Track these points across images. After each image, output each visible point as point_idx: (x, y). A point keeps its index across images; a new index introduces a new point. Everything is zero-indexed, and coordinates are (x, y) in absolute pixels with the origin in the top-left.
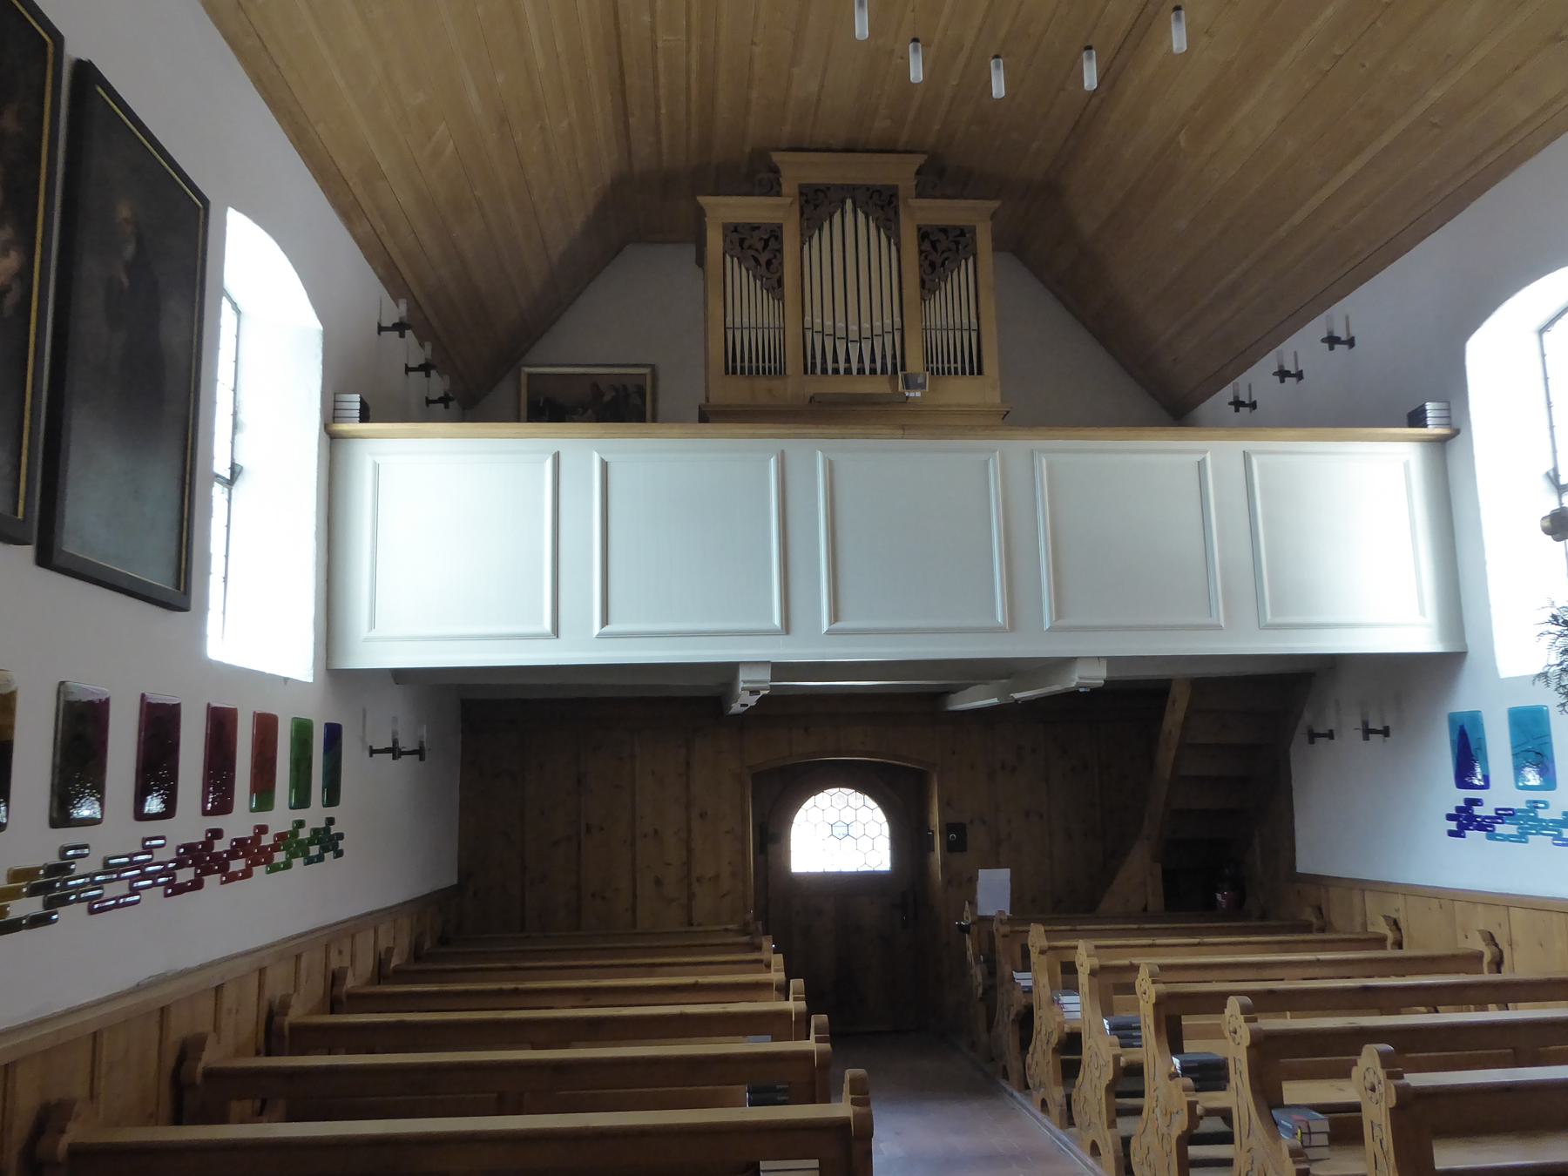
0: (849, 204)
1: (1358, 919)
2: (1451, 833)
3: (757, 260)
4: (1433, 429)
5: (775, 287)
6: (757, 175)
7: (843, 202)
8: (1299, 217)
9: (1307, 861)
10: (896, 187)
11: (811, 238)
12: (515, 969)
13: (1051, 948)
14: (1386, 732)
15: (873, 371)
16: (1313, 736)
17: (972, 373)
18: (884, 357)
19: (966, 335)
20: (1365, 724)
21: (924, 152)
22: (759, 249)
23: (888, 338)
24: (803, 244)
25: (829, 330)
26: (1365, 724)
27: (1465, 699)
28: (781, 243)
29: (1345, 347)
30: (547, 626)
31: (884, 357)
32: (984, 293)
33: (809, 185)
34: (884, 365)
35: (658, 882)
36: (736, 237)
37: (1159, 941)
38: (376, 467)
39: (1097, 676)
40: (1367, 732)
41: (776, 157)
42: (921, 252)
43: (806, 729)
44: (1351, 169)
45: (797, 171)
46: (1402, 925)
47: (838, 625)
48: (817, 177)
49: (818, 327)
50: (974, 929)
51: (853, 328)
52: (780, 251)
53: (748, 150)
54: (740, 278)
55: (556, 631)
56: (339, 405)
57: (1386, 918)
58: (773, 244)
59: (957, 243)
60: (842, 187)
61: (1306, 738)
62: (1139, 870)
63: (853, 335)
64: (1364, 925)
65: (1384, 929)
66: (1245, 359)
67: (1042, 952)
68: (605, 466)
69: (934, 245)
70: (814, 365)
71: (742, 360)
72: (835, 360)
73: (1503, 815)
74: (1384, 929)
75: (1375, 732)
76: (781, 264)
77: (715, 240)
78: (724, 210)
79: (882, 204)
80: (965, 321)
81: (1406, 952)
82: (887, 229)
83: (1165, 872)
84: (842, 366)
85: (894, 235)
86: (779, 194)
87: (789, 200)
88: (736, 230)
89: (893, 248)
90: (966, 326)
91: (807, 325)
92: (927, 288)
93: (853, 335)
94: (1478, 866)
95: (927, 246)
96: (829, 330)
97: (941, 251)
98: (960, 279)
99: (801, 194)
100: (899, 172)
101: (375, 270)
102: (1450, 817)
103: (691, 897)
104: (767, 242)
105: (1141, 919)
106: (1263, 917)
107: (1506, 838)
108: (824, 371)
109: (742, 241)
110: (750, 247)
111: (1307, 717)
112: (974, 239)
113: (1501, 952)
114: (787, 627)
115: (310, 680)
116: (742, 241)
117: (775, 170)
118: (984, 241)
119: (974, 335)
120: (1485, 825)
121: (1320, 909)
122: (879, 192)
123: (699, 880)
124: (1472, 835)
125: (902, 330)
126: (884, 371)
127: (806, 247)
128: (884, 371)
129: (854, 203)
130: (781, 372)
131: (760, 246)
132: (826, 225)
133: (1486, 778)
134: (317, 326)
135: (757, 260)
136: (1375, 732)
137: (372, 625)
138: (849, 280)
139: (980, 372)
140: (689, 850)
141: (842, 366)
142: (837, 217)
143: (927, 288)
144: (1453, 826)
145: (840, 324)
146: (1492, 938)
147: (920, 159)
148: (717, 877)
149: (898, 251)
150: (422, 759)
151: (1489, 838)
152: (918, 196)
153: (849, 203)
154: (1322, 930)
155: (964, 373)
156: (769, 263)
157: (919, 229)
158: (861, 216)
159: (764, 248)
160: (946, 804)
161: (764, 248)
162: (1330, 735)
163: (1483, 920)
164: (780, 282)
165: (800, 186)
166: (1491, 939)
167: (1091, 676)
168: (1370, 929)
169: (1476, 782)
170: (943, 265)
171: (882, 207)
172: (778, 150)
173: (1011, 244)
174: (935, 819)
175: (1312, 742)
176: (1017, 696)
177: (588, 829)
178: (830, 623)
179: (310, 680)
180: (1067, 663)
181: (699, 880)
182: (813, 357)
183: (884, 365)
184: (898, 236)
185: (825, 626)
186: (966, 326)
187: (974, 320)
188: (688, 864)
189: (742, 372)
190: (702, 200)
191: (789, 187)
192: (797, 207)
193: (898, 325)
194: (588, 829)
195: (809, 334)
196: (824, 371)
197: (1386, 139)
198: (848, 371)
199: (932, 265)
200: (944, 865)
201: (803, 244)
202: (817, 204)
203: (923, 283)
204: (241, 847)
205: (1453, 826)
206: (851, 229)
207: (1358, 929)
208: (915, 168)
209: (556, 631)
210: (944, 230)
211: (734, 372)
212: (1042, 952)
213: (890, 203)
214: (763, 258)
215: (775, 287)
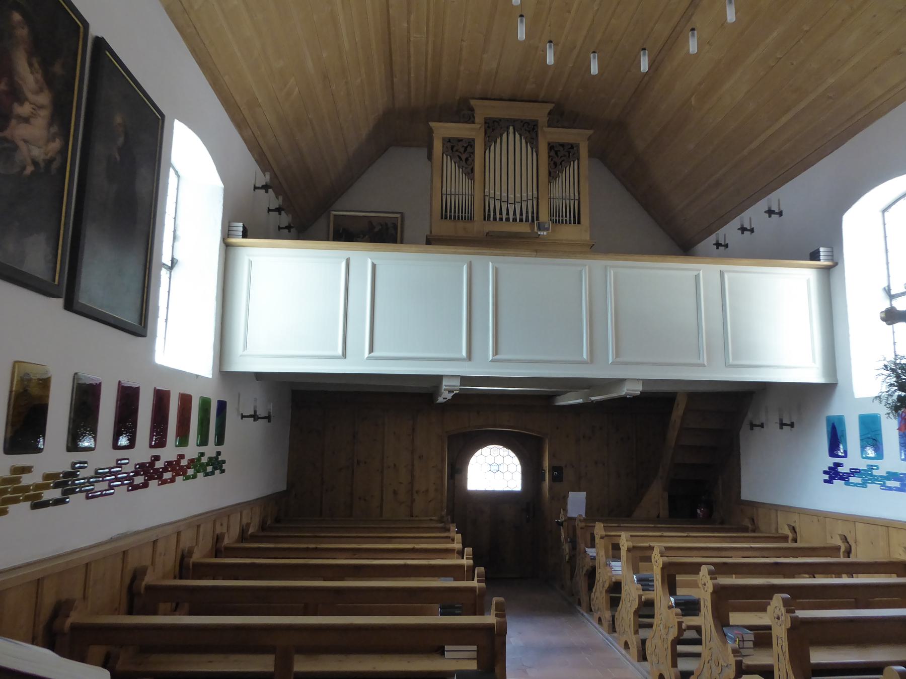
2: (826, 481)
4: (823, 262)
5: (470, 173)
6: (462, 112)
7: (508, 128)
8: (753, 146)
9: (746, 495)
11: (490, 147)
13: (607, 536)
14: (792, 425)
15: (521, 220)
16: (752, 426)
17: (574, 223)
18: (527, 212)
19: (572, 202)
20: (781, 420)
22: (462, 152)
23: (530, 203)
24: (485, 150)
26: (781, 420)
30: (340, 352)
31: (527, 212)
32: (584, 180)
33: (490, 118)
34: (527, 217)
35: (395, 493)
36: (449, 145)
39: (636, 389)
40: (782, 425)
42: (549, 157)
44: (784, 119)
45: (484, 110)
46: (797, 530)
47: (497, 357)
49: (492, 195)
52: (473, 153)
53: (458, 98)
54: (451, 167)
57: (789, 525)
58: (469, 149)
59: (569, 152)
60: (508, 120)
62: (656, 495)
63: (511, 200)
64: (777, 529)
65: (787, 532)
66: (723, 220)
67: (602, 538)
68: (374, 266)
69: (556, 153)
70: (489, 215)
72: (501, 214)
74: (787, 532)
76: (473, 160)
77: (438, 146)
78: (444, 130)
79: (529, 130)
80: (572, 195)
82: (532, 143)
84: (498, 216)
86: (473, 122)
87: (478, 126)
90: (572, 197)
91: (487, 194)
92: (552, 176)
93: (511, 200)
95: (553, 153)
97: (560, 157)
98: (570, 172)
99: (485, 123)
100: (540, 113)
102: (825, 472)
103: (413, 501)
104: (466, 148)
105: (656, 522)
106: (722, 523)
108: (495, 219)
109: (452, 147)
111: (750, 415)
112: (578, 150)
114: (469, 357)
116: (452, 147)
117: (472, 110)
118: (584, 152)
119: (576, 203)
120: (844, 477)
123: (417, 492)
126: (527, 220)
128: (527, 220)
130: (471, 219)
131: (462, 150)
132: (499, 140)
133: (845, 452)
137: (245, 348)
139: (579, 223)
140: (413, 476)
142: (505, 136)
143: (552, 176)
144: (827, 477)
147: (550, 106)
148: (427, 491)
149: (537, 155)
152: (549, 126)
153: (511, 129)
154: (754, 531)
155: (570, 223)
156: (467, 159)
158: (517, 136)
160: (552, 456)
162: (762, 426)
164: (472, 170)
165: (485, 119)
167: (633, 389)
173: (599, 153)
174: (546, 464)
175: (752, 429)
176: (593, 398)
177: (358, 462)
179: (210, 376)
180: (620, 382)
181: (417, 492)
183: (527, 217)
184: (537, 148)
186: (572, 197)
187: (576, 194)
188: (412, 483)
189: (450, 218)
190: (432, 124)
191: (479, 119)
193: (535, 196)
194: (358, 462)
195: (487, 199)
196: (495, 219)
197: (803, 105)
199: (555, 164)
200: (550, 488)
201: (485, 150)
202: (494, 129)
203: (550, 174)
206: (511, 143)
207: (774, 531)
210: (562, 145)
211: (446, 218)
212: (602, 538)
214: (464, 157)
215: (470, 173)
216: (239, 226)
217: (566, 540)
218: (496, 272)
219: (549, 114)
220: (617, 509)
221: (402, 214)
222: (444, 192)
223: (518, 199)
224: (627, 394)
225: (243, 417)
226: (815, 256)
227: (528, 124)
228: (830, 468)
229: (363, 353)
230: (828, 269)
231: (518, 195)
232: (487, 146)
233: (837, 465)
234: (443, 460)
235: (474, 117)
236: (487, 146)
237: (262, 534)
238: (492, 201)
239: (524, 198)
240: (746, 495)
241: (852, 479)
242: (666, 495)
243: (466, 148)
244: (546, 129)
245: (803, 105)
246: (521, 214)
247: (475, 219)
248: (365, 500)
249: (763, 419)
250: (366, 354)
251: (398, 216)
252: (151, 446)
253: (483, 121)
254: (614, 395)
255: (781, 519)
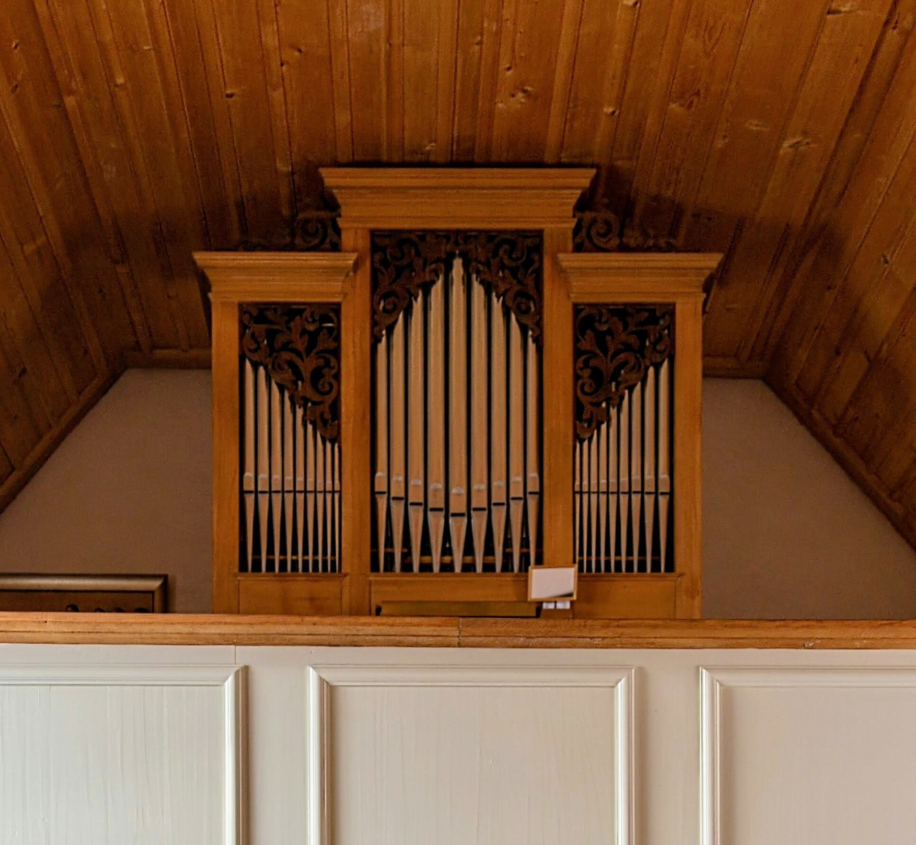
5: (326, 421)
6: (307, 221)
7: (449, 268)
11: (390, 330)
15: (489, 568)
17: (656, 567)
18: (508, 543)
19: (649, 500)
21: (592, 166)
22: (294, 345)
25: (416, 496)
31: (508, 543)
32: (705, 441)
34: (508, 557)
36: (260, 328)
41: (332, 178)
45: (371, 203)
48: (402, 215)
51: (458, 490)
52: (336, 353)
53: (283, 167)
54: (268, 403)
58: (324, 343)
59: (643, 336)
60: (448, 235)
63: (458, 504)
70: (390, 557)
71: (271, 551)
72: (426, 549)
76: (337, 377)
77: (225, 331)
78: (246, 277)
79: (511, 265)
80: (649, 477)
82: (522, 312)
84: (436, 559)
86: (336, 248)
89: (532, 347)
91: (381, 486)
93: (458, 504)
95: (587, 344)
98: (643, 402)
99: (375, 248)
100: (544, 204)
104: (313, 338)
108: (407, 567)
110: (286, 347)
117: (331, 204)
118: (689, 333)
119: (663, 501)
122: (512, 244)
126: (507, 566)
127: (382, 347)
129: (466, 266)
130: (334, 568)
131: (301, 344)
132: (418, 305)
138: (456, 387)
139: (670, 567)
141: (436, 559)
142: (437, 290)
143: (587, 418)
147: (583, 178)
152: (578, 248)
153: (458, 264)
155: (642, 567)
156: (317, 375)
158: (478, 290)
159: (309, 350)
161: (309, 350)
165: (375, 234)
170: (615, 376)
171: (514, 272)
172: (337, 164)
173: (759, 361)
183: (508, 557)
184: (539, 325)
187: (664, 476)
189: (270, 566)
190: (201, 257)
191: (353, 236)
193: (533, 486)
196: (407, 567)
198: (447, 568)
199: (597, 376)
201: (375, 340)
202: (402, 266)
203: (578, 409)
206: (458, 313)
211: (257, 567)
213: (529, 263)
214: (307, 366)
221: (165, 578)
223: (480, 500)
231: (479, 486)
232: (380, 328)
235: (338, 231)
236: (380, 328)
238: (398, 510)
243: (313, 338)
244: (569, 260)
246: (489, 549)
251: (155, 584)
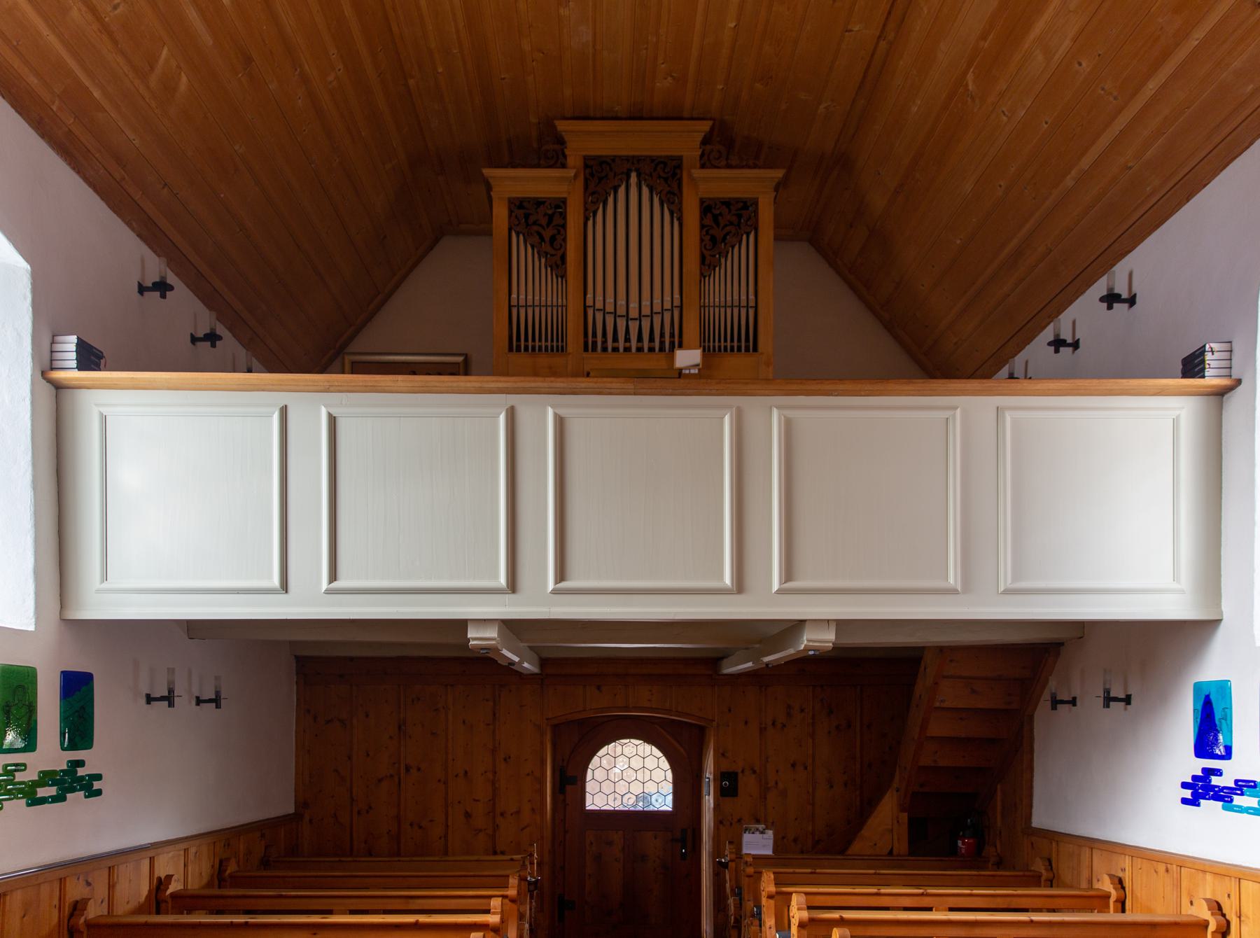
0: (634, 178)
1: (1085, 874)
2: (1185, 801)
3: (542, 238)
4: (1212, 378)
5: (558, 265)
6: (548, 151)
8: (1086, 162)
9: (1040, 820)
10: (680, 158)
12: (281, 897)
14: (1127, 700)
15: (651, 350)
16: (1055, 703)
17: (747, 350)
18: (662, 335)
19: (743, 311)
20: (1107, 691)
22: (541, 224)
23: (667, 316)
24: (586, 219)
25: (610, 308)
26: (1107, 691)
27: (1213, 666)
28: (565, 218)
29: (1126, 305)
30: (276, 582)
31: (662, 335)
33: (595, 158)
34: (662, 343)
35: (468, 815)
37: (883, 891)
38: (104, 419)
39: (825, 639)
40: (1108, 700)
41: (562, 126)
42: (702, 226)
43: (599, 688)
44: (1152, 86)
46: (1127, 884)
47: (563, 585)
49: (599, 305)
50: (732, 865)
52: (564, 226)
53: (534, 120)
54: (523, 253)
55: (285, 586)
56: (58, 347)
57: (1111, 876)
58: (557, 220)
59: (739, 216)
60: (627, 159)
61: (1049, 704)
62: (887, 819)
63: (634, 314)
64: (1090, 882)
65: (1107, 886)
66: (1024, 336)
67: (770, 897)
68: (333, 421)
69: (716, 219)
70: (594, 343)
72: (615, 339)
73: (1242, 786)
74: (1107, 886)
75: (1116, 699)
76: (564, 240)
78: (514, 182)
79: (665, 176)
80: (743, 297)
81: (1128, 917)
82: (671, 203)
83: (912, 823)
84: (610, 345)
85: (677, 214)
86: (564, 166)
87: (572, 173)
88: (521, 207)
90: (744, 303)
92: (708, 264)
93: (634, 314)
94: (1211, 835)
96: (610, 308)
97: (725, 225)
98: (741, 254)
99: (586, 166)
100: (682, 141)
101: (129, 224)
102: (1185, 785)
103: (496, 827)
104: (551, 218)
105: (887, 864)
106: (999, 864)
107: (1241, 810)
108: (605, 349)
109: (527, 216)
110: (535, 223)
111: (1052, 685)
112: (756, 212)
113: (1228, 923)
114: (513, 586)
115: (32, 628)
116: (527, 216)
117: (561, 141)
119: (751, 312)
120: (1223, 796)
121: (1050, 861)
123: (502, 814)
124: (1210, 807)
125: (681, 307)
126: (662, 349)
127: (590, 223)
128: (662, 349)
129: (639, 176)
131: (544, 222)
132: (611, 200)
133: (1228, 750)
134: (23, 265)
135: (542, 238)
136: (1116, 699)
137: (105, 577)
139: (755, 349)
141: (621, 345)
143: (708, 264)
144: (1188, 794)
145: (622, 302)
146: (1220, 908)
147: (706, 126)
148: (518, 812)
149: (681, 225)
150: (218, 706)
151: (1224, 808)
152: (703, 166)
154: (1050, 883)
155: (739, 349)
156: (553, 239)
157: (702, 201)
158: (645, 191)
160: (721, 755)
162: (1073, 702)
163: (1209, 888)
164: (563, 258)
165: (586, 158)
166: (1218, 908)
167: (819, 639)
168: (1096, 885)
169: (1217, 752)
170: (724, 239)
171: (666, 180)
173: (806, 231)
174: (709, 773)
175: (1054, 708)
176: (767, 659)
177: (408, 769)
178: (556, 583)
179: (32, 628)
180: (798, 625)
181: (502, 814)
182: (594, 335)
183: (662, 343)
185: (551, 585)
186: (744, 303)
187: (752, 297)
189: (526, 349)
191: (574, 160)
192: (580, 184)
193: (677, 303)
194: (408, 769)
195: (590, 312)
196: (605, 349)
197: (1199, 35)
200: (717, 807)
201: (586, 219)
202: (602, 176)
203: (703, 258)
204: (47, 777)
205: (1188, 794)
206: (634, 204)
207: (1084, 885)
208: (699, 137)
209: (285, 586)
210: (727, 203)
211: (518, 349)
212: (770, 897)
214: (547, 234)
215: (558, 265)
216: (69, 344)
217: (732, 890)
218: (560, 423)
219: (705, 141)
220: (820, 846)
222: (514, 302)
223: (646, 311)
224: (807, 649)
225: (199, 701)
226: (1193, 366)
227: (665, 164)
228: (1194, 777)
229: (320, 583)
230: (1221, 393)
231: (646, 303)
232: (589, 213)
233: (1209, 772)
234: (543, 762)
235: (565, 157)
236: (589, 213)
237: (216, 892)
238: (599, 316)
239: (657, 308)
240: (1040, 820)
241: (1237, 800)
242: (904, 817)
244: (698, 173)
245: (1199, 35)
247: (570, 349)
248: (420, 827)
249: (1076, 692)
250: (325, 584)
251: (460, 359)
252: (63, 749)
253: (580, 163)
254: (791, 651)
255: (1098, 861)
